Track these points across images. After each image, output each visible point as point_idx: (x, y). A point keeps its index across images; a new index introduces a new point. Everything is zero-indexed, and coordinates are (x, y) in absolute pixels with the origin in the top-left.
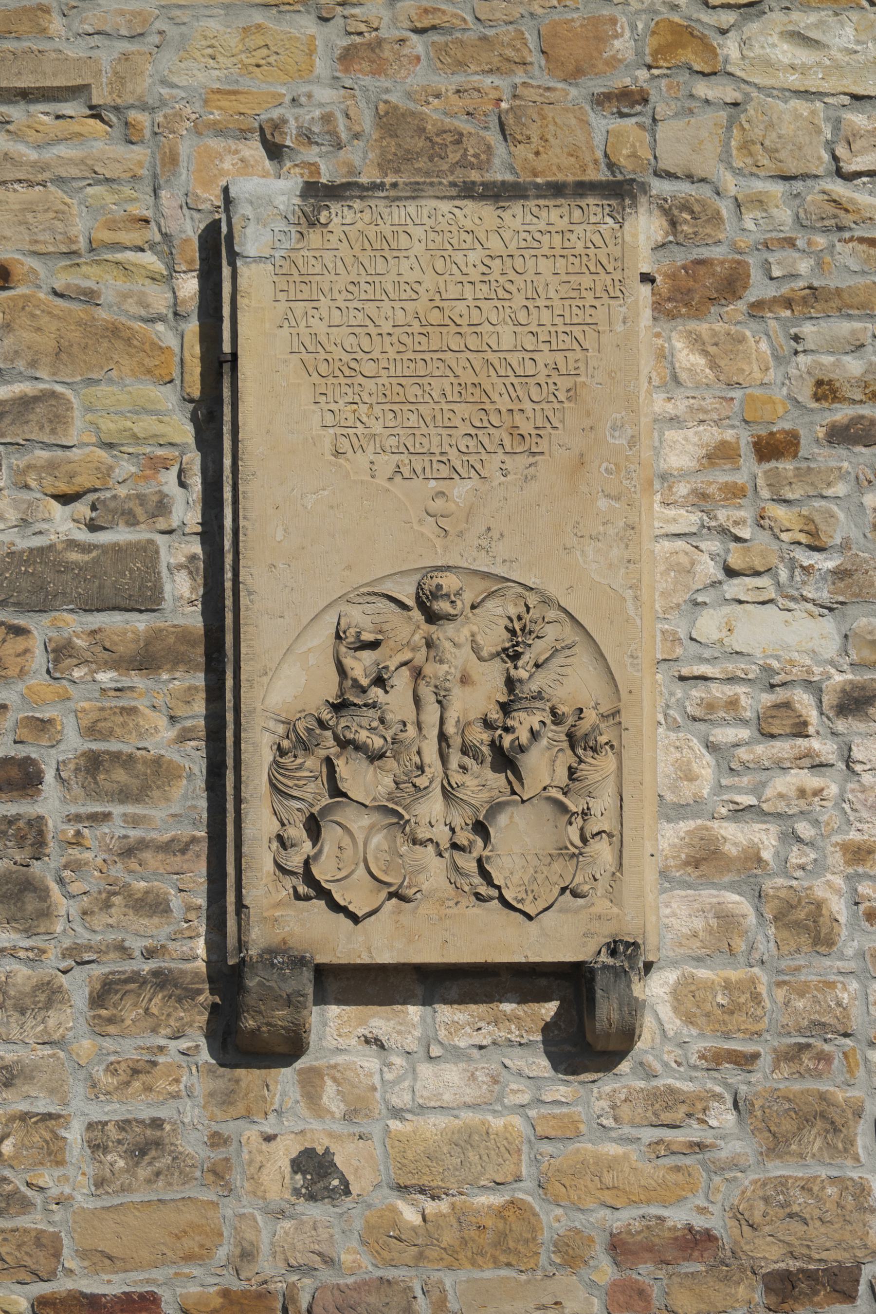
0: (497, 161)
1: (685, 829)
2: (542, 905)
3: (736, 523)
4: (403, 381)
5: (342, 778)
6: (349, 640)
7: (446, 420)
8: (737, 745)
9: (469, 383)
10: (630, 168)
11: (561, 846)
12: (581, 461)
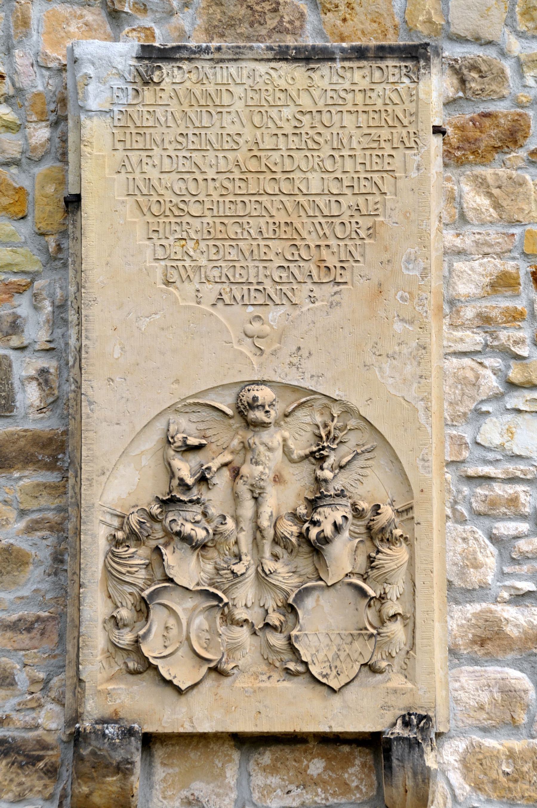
0: (308, 27)
1: (472, 611)
2: (344, 680)
3: (516, 343)
4: (226, 221)
5: (169, 566)
6: (175, 445)
7: (262, 254)
8: (517, 537)
9: (282, 222)
10: (426, 32)
11: (361, 626)
12: (380, 289)
